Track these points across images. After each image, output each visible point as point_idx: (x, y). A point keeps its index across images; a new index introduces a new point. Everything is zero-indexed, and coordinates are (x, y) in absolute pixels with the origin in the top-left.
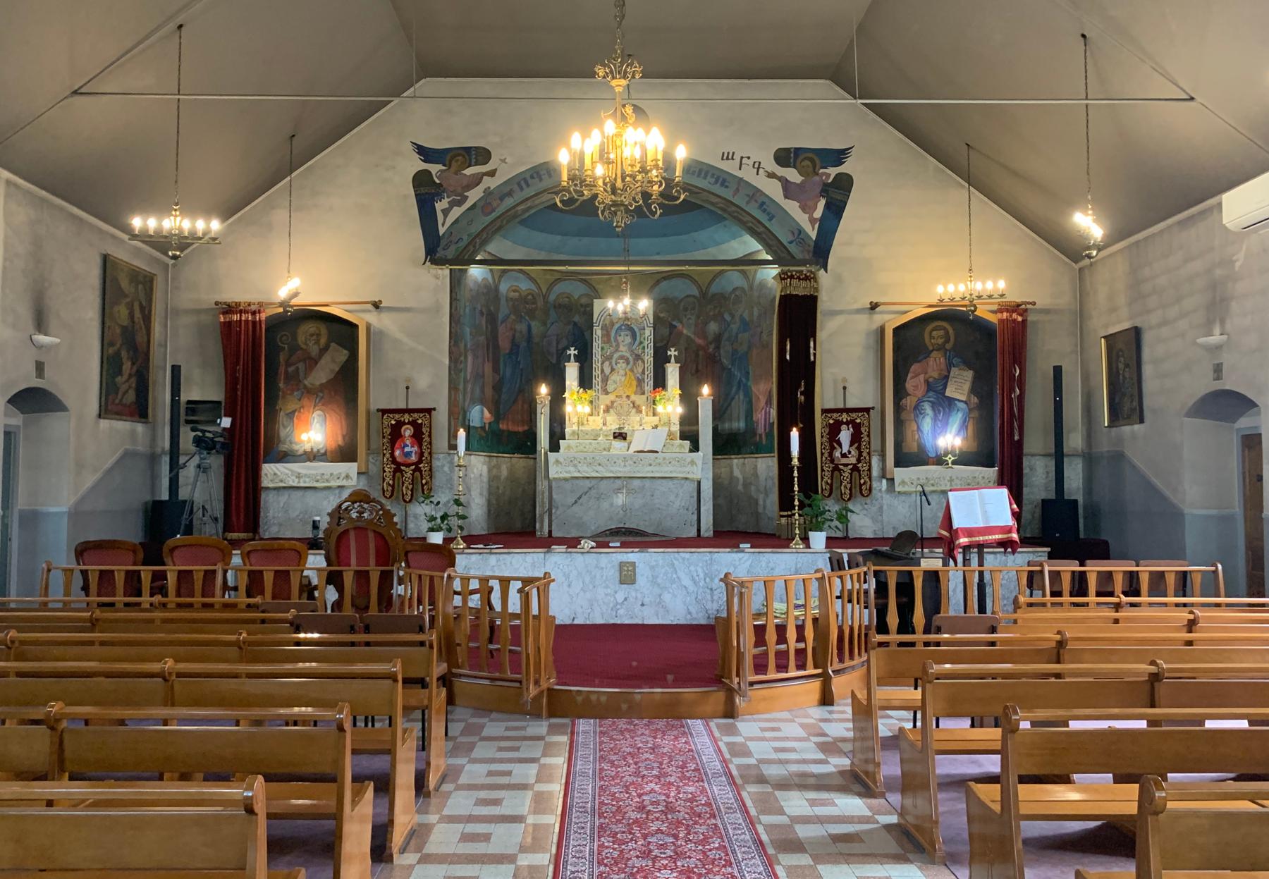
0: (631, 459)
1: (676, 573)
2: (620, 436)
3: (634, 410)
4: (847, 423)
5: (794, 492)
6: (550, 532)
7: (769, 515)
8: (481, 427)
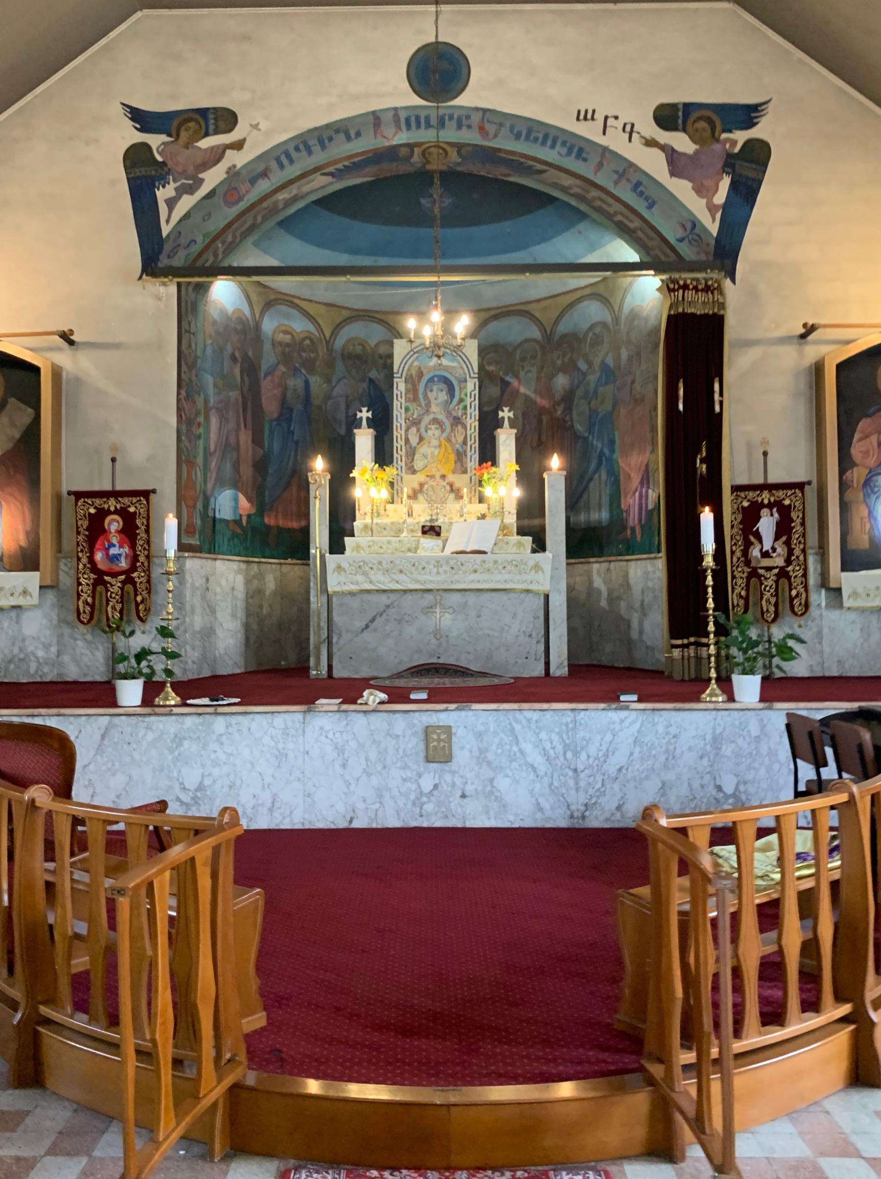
1: (517, 743)
2: (432, 530)
3: (452, 496)
4: (770, 506)
5: (707, 610)
6: (330, 667)
7: (649, 643)
8: (235, 521)
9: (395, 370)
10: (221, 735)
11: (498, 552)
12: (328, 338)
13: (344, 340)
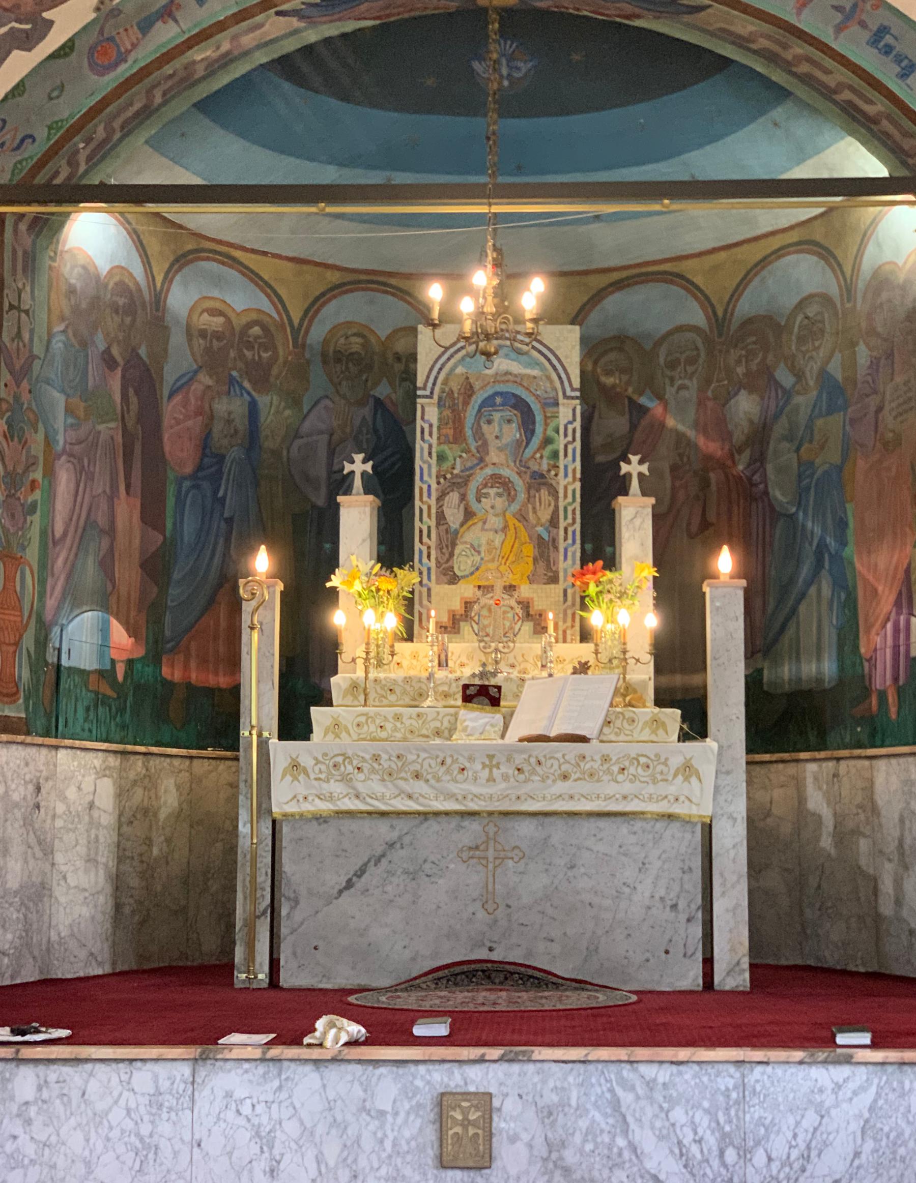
0: (509, 759)
1: (626, 1132)
3: (528, 627)
6: (274, 965)
8: (101, 673)
9: (420, 383)
10: (27, 1103)
11: (612, 737)
12: (296, 322)
13: (328, 327)
